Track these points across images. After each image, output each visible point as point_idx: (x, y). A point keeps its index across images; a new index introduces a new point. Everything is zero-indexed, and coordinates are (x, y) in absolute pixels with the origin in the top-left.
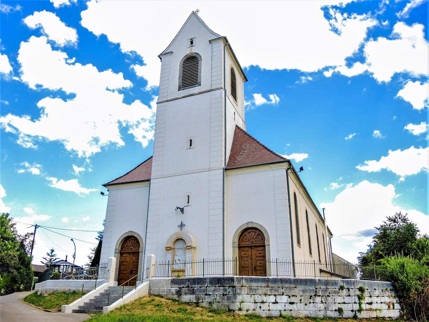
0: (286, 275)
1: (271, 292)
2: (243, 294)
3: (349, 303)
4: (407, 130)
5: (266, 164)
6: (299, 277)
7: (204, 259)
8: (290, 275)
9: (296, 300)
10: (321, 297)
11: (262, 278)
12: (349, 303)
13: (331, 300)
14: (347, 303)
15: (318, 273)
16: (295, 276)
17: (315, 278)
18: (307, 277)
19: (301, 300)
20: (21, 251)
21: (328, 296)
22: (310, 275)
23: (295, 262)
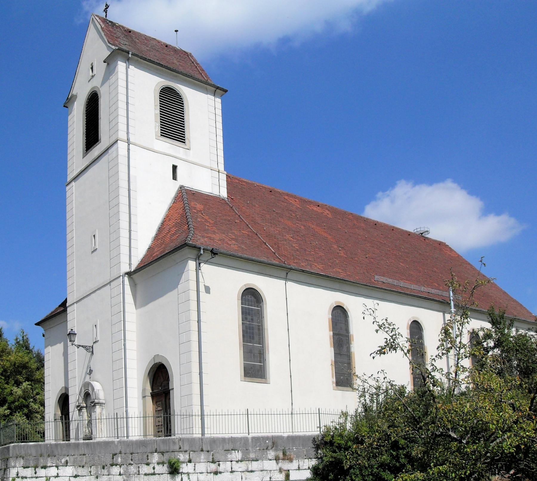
0: (134, 435)
1: (52, 463)
2: (18, 466)
3: (162, 474)
4: (60, 343)
5: (420, 297)
6: (212, 435)
7: (247, 409)
8: (134, 435)
9: (84, 473)
10: (118, 466)
11: (34, 444)
12: (162, 474)
13: (134, 470)
14: (159, 474)
15: (150, 429)
16: (127, 437)
17: (249, 435)
18: (294, 434)
19: (90, 472)
20: (436, 389)
21: (130, 464)
22: (239, 432)
23: (205, 414)
